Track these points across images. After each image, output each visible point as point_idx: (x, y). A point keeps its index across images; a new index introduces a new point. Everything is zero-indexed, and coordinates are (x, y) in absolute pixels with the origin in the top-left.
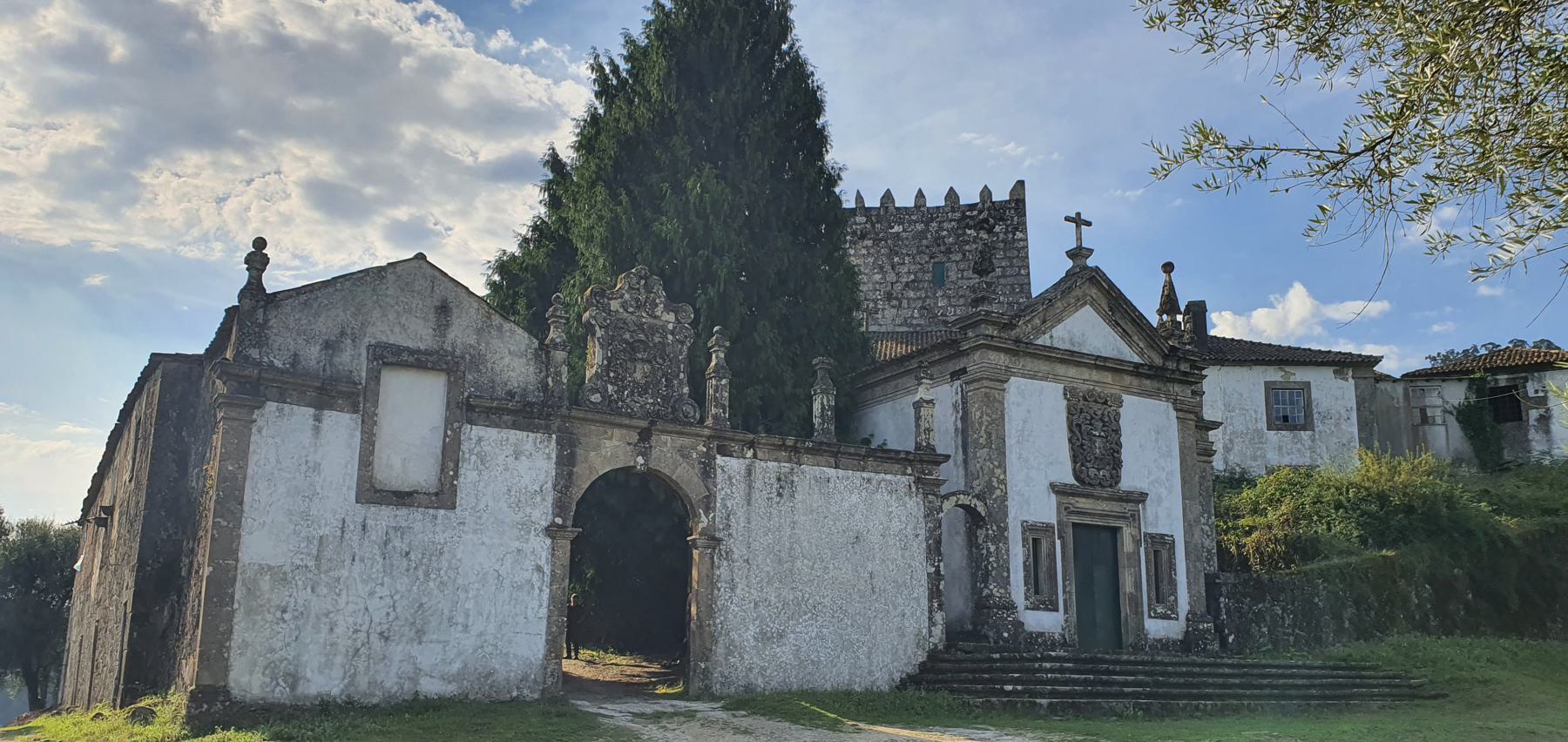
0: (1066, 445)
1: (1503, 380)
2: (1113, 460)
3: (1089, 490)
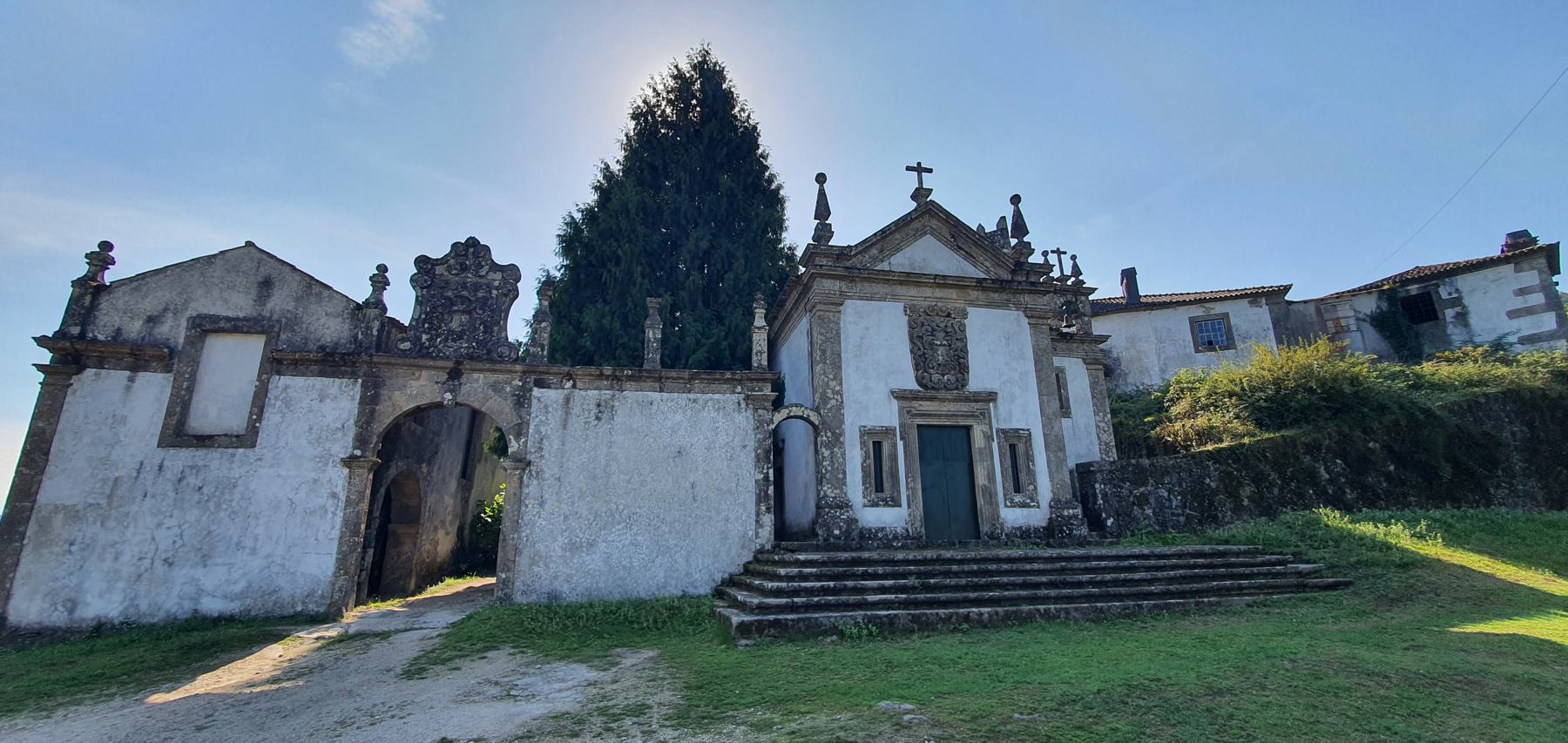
0: (909, 355)
1: (1414, 289)
2: (959, 363)
3: (933, 393)
